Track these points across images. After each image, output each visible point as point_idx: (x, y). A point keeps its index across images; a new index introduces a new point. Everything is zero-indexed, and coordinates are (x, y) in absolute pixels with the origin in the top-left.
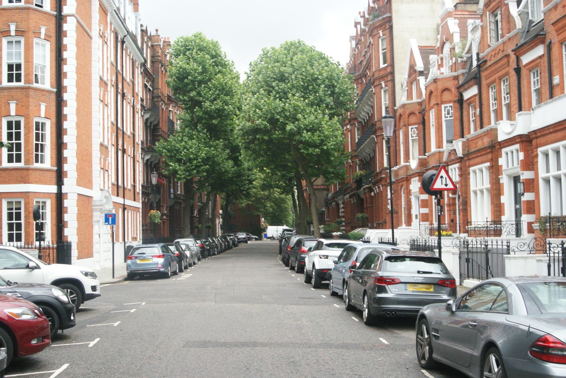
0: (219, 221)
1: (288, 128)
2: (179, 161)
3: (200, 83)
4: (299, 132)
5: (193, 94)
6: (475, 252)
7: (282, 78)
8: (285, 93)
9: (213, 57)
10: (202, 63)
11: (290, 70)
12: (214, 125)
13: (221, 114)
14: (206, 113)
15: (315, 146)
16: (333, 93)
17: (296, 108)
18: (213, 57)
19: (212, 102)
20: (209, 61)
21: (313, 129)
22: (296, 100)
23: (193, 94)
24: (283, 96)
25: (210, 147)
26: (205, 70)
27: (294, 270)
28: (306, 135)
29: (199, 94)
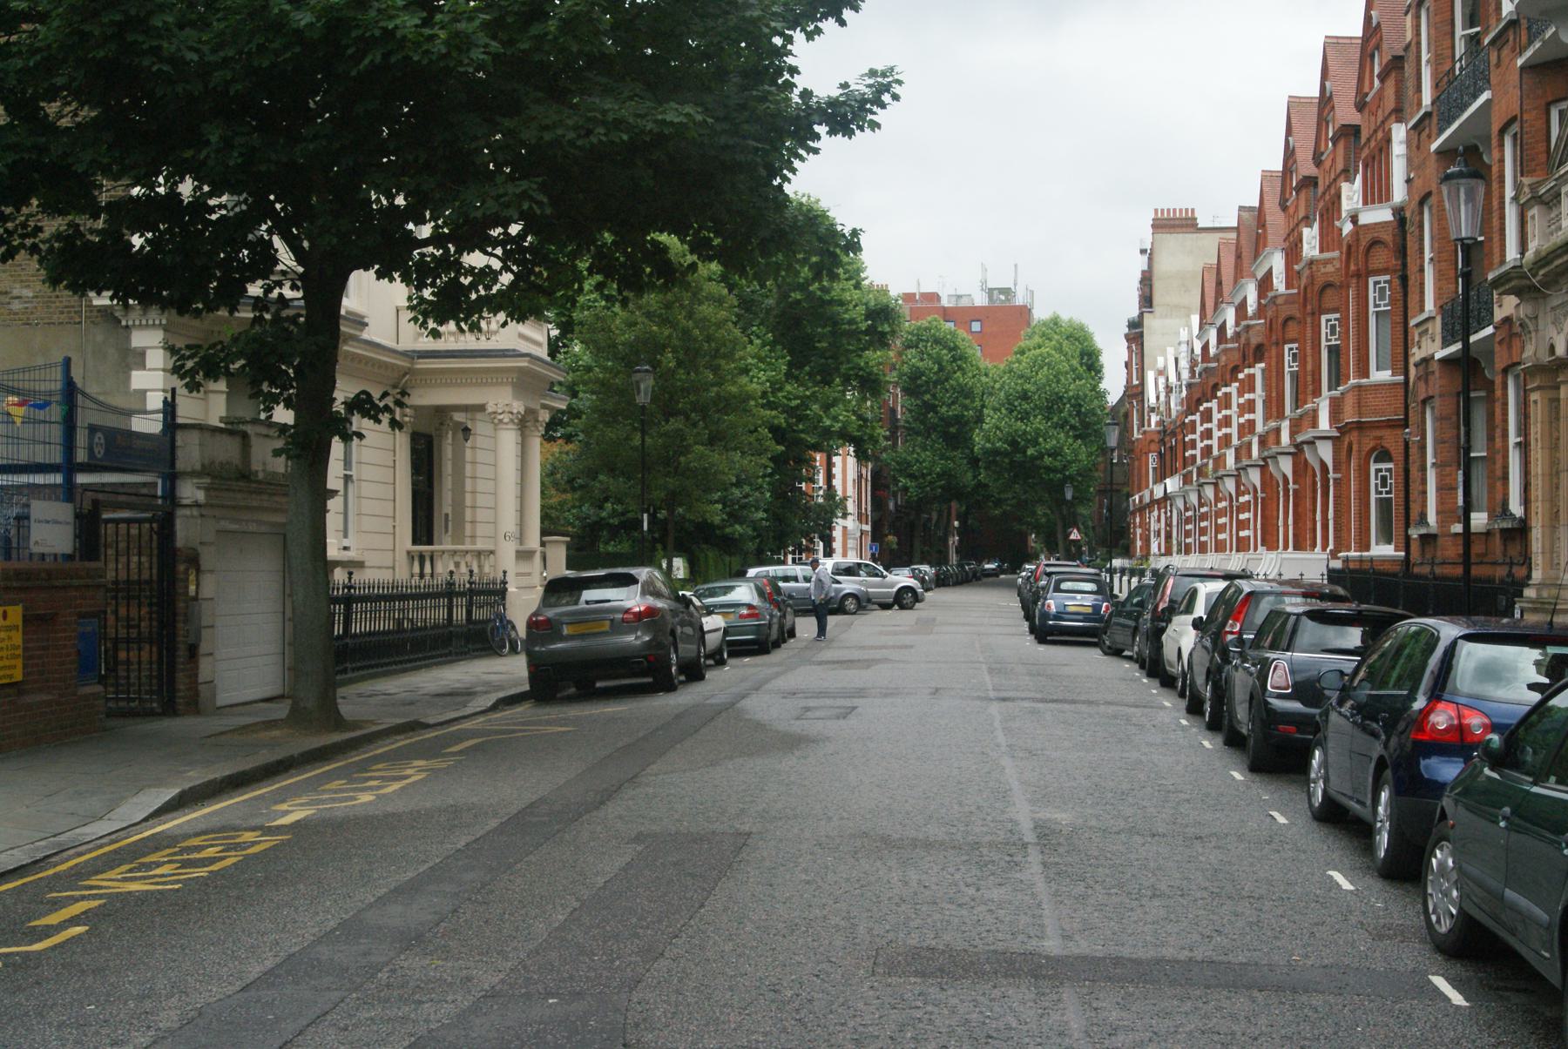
0: (954, 540)
1: (1029, 452)
2: (912, 476)
3: (936, 383)
4: (1041, 456)
5: (927, 397)
6: (40, 442)
7: (1025, 396)
8: (1027, 413)
9: (951, 350)
10: (938, 361)
11: (1033, 389)
12: (955, 434)
13: (958, 420)
14: (942, 419)
15: (1055, 470)
16: (1079, 413)
17: (1037, 431)
18: (951, 350)
19: (949, 406)
20: (946, 356)
21: (1055, 453)
22: (1038, 422)
23: (927, 397)
24: (1024, 417)
25: (947, 459)
26: (941, 369)
27: (1202, 714)
28: (1048, 460)
29: (934, 396)
